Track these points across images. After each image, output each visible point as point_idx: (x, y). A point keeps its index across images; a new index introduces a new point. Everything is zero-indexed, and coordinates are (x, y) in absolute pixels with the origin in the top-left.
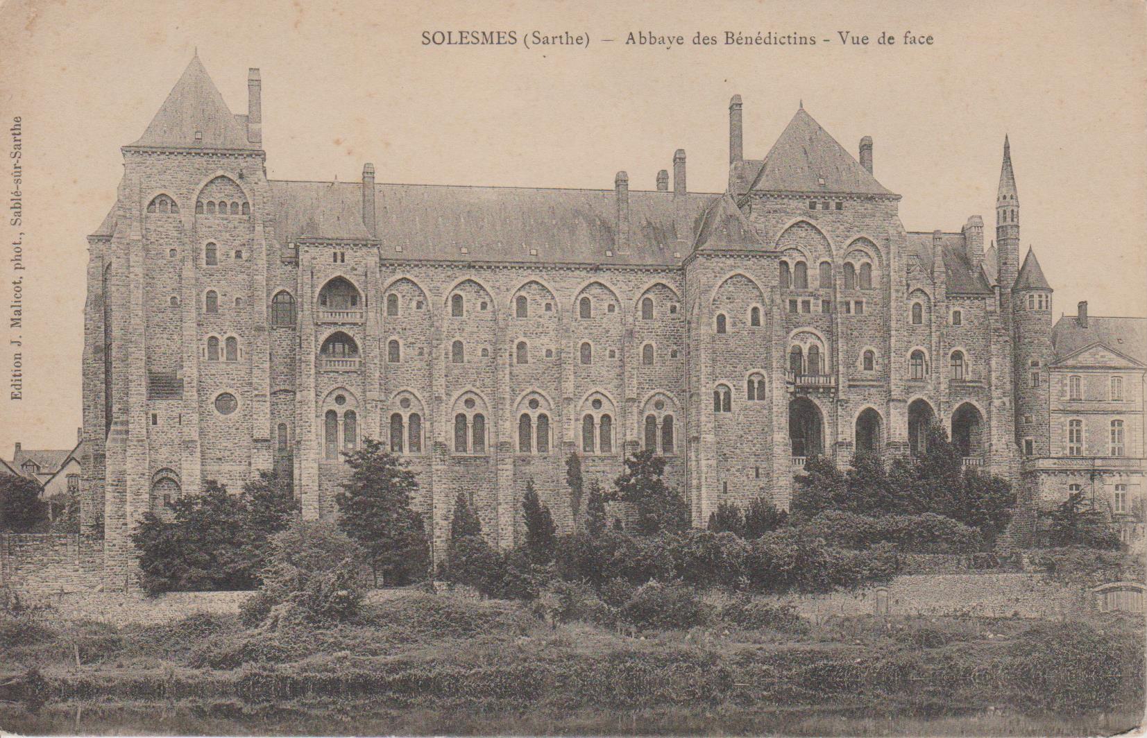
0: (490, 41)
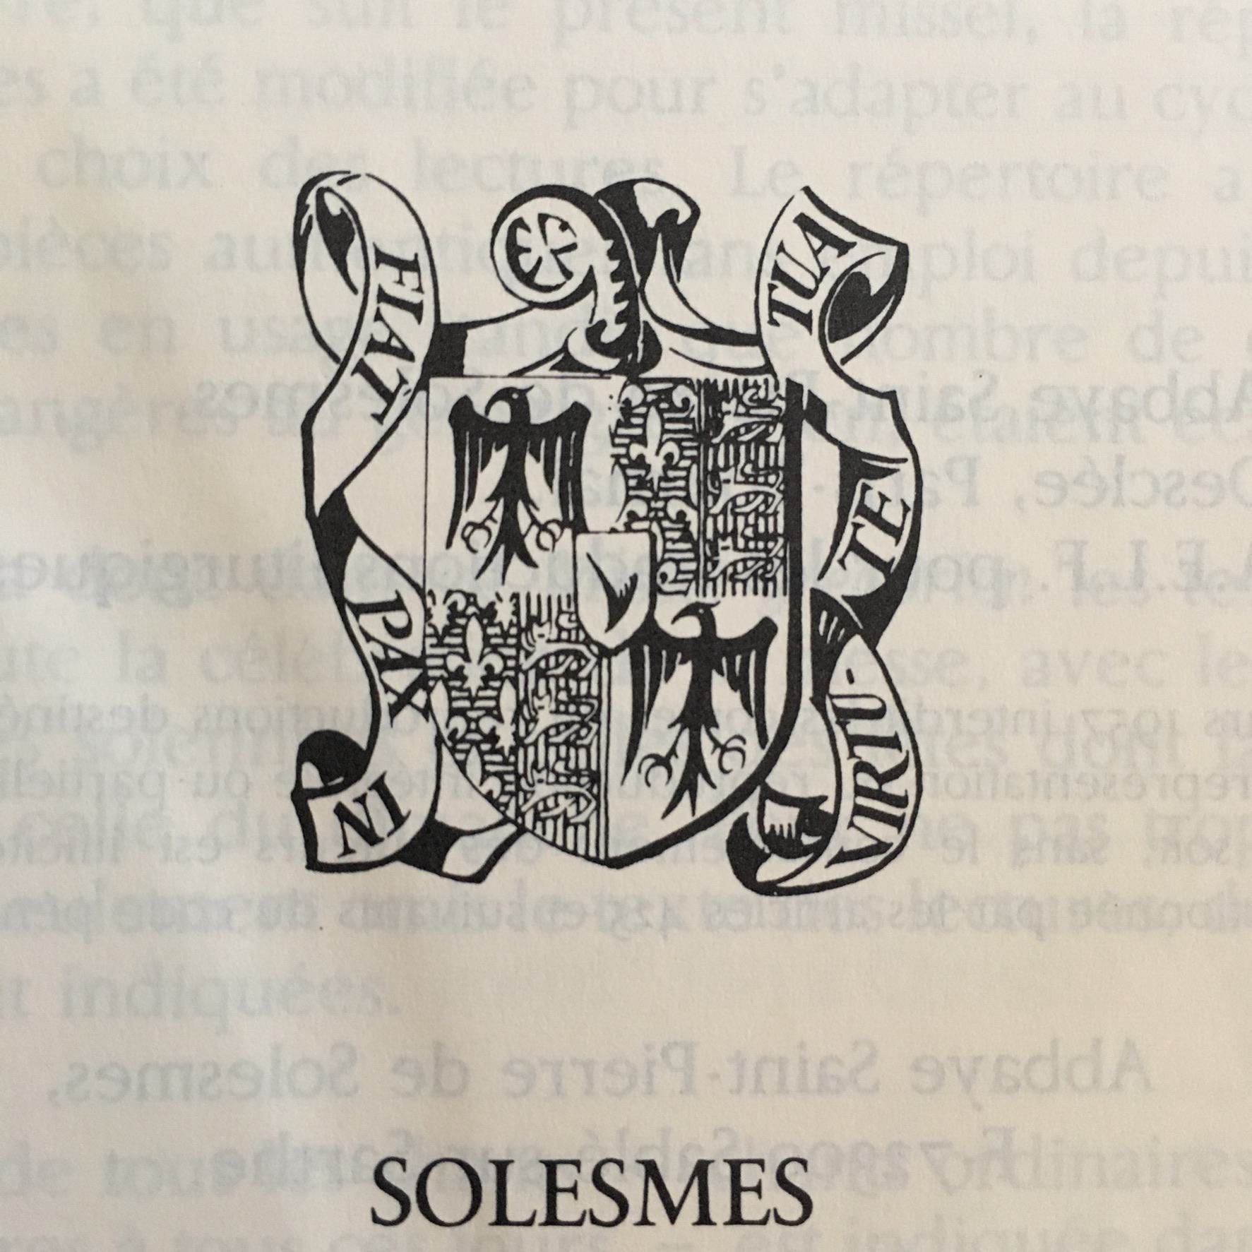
0: (691, 1210)
